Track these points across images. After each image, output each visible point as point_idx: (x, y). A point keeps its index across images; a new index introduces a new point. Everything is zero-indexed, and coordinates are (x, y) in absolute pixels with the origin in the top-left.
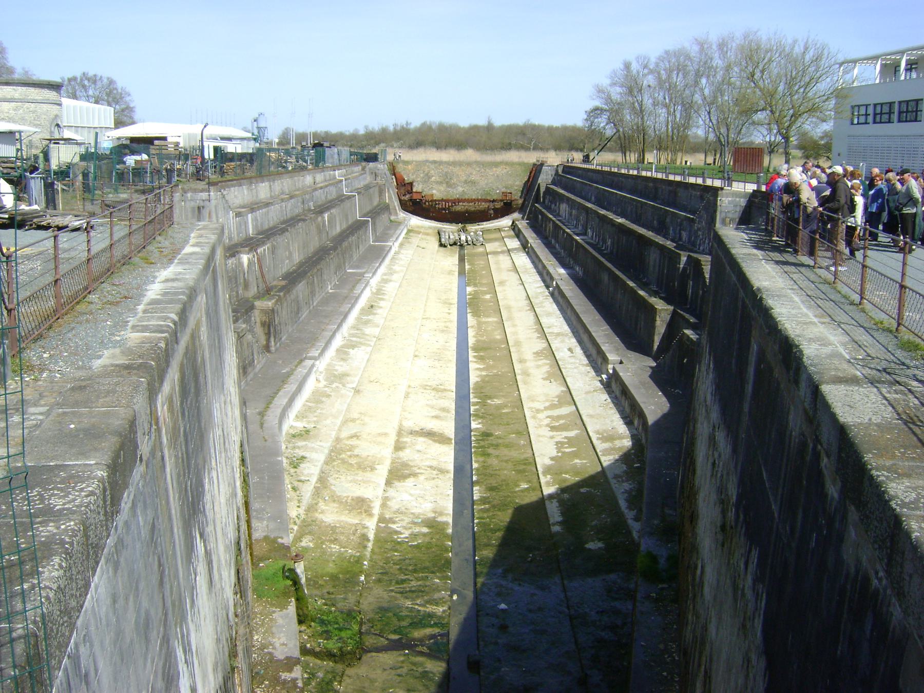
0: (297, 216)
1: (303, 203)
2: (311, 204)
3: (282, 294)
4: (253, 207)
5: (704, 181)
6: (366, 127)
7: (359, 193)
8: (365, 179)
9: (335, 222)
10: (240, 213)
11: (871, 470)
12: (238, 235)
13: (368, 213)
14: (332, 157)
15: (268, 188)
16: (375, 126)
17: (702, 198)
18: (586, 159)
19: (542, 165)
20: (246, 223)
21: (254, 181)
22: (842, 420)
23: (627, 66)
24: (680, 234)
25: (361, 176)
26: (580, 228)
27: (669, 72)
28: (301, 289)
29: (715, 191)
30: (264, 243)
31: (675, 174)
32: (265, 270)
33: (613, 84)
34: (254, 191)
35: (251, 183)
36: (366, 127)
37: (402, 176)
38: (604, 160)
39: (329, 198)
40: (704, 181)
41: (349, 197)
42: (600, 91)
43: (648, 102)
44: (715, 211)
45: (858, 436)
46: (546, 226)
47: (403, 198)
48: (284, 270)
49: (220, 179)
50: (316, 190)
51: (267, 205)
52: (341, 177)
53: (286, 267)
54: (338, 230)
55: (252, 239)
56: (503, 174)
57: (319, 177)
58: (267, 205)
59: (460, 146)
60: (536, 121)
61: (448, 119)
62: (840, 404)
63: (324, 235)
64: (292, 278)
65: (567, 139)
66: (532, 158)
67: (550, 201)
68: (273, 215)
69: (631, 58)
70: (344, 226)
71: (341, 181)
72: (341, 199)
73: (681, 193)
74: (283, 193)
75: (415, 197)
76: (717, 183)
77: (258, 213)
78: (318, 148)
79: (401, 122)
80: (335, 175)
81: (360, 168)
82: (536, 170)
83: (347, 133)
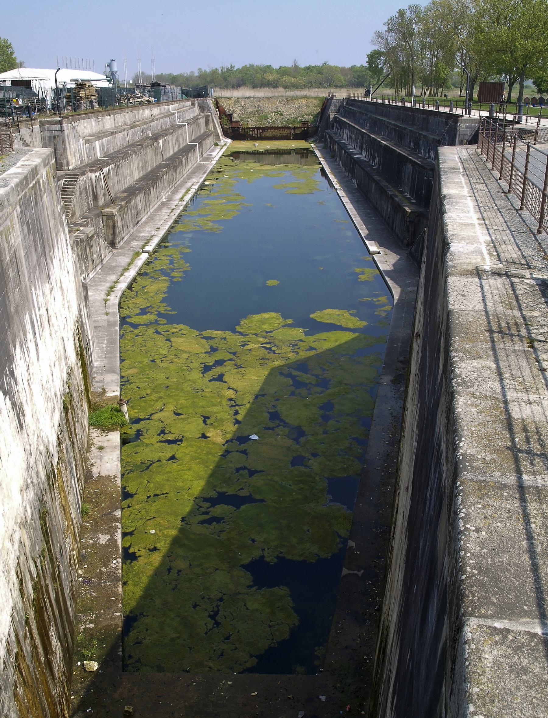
0: (137, 142)
1: (142, 131)
2: (149, 132)
3: (123, 203)
4: (99, 136)
5: (451, 110)
6: (200, 70)
7: (189, 124)
8: (194, 112)
9: (170, 147)
10: (89, 140)
11: (452, 351)
12: (88, 158)
13: (196, 139)
14: (167, 95)
15: (112, 120)
16: (207, 68)
17: (447, 123)
18: (367, 94)
19: (332, 98)
20: (94, 148)
21: (100, 114)
22: (451, 307)
23: (401, 14)
24: (429, 153)
25: (189, 110)
26: (357, 148)
27: (435, 19)
28: (139, 199)
29: (457, 117)
30: (108, 164)
31: (444, 106)
32: (110, 184)
33: (390, 30)
34: (101, 123)
35: (98, 116)
36: (200, 70)
37: (224, 109)
38: (386, 95)
39: (164, 127)
40: (451, 110)
41: (180, 127)
42: (379, 35)
43: (416, 46)
44: (455, 135)
45: (456, 320)
46: (333, 147)
47: (225, 126)
48: (127, 185)
49: (74, 113)
50: (152, 121)
51: (113, 133)
52: (184, 110)
53: (129, 182)
54: (171, 153)
55: (99, 160)
56: (302, 106)
57: (156, 111)
58: (113, 133)
59: (274, 85)
60: (333, 62)
61: (259, 61)
62: (455, 293)
63: (159, 157)
64: (131, 192)
65: (356, 78)
66: (324, 93)
67: (337, 128)
68: (119, 141)
69: (405, 7)
70: (176, 150)
71: (174, 114)
72: (174, 128)
73: (431, 118)
74: (125, 124)
75: (234, 125)
76: (459, 112)
77: (104, 140)
78: (156, 89)
79: (227, 65)
80: (169, 109)
81: (191, 103)
82: (326, 103)
83: (185, 75)
